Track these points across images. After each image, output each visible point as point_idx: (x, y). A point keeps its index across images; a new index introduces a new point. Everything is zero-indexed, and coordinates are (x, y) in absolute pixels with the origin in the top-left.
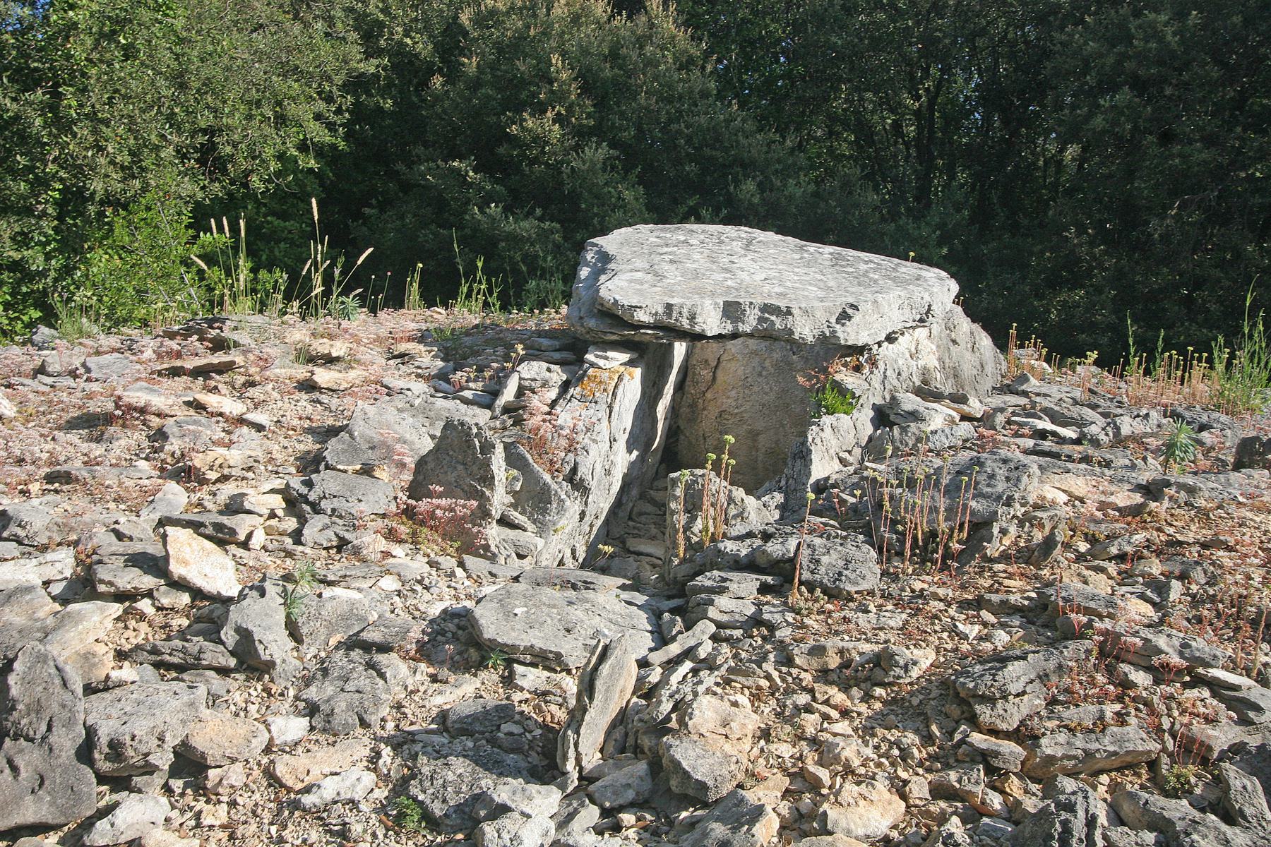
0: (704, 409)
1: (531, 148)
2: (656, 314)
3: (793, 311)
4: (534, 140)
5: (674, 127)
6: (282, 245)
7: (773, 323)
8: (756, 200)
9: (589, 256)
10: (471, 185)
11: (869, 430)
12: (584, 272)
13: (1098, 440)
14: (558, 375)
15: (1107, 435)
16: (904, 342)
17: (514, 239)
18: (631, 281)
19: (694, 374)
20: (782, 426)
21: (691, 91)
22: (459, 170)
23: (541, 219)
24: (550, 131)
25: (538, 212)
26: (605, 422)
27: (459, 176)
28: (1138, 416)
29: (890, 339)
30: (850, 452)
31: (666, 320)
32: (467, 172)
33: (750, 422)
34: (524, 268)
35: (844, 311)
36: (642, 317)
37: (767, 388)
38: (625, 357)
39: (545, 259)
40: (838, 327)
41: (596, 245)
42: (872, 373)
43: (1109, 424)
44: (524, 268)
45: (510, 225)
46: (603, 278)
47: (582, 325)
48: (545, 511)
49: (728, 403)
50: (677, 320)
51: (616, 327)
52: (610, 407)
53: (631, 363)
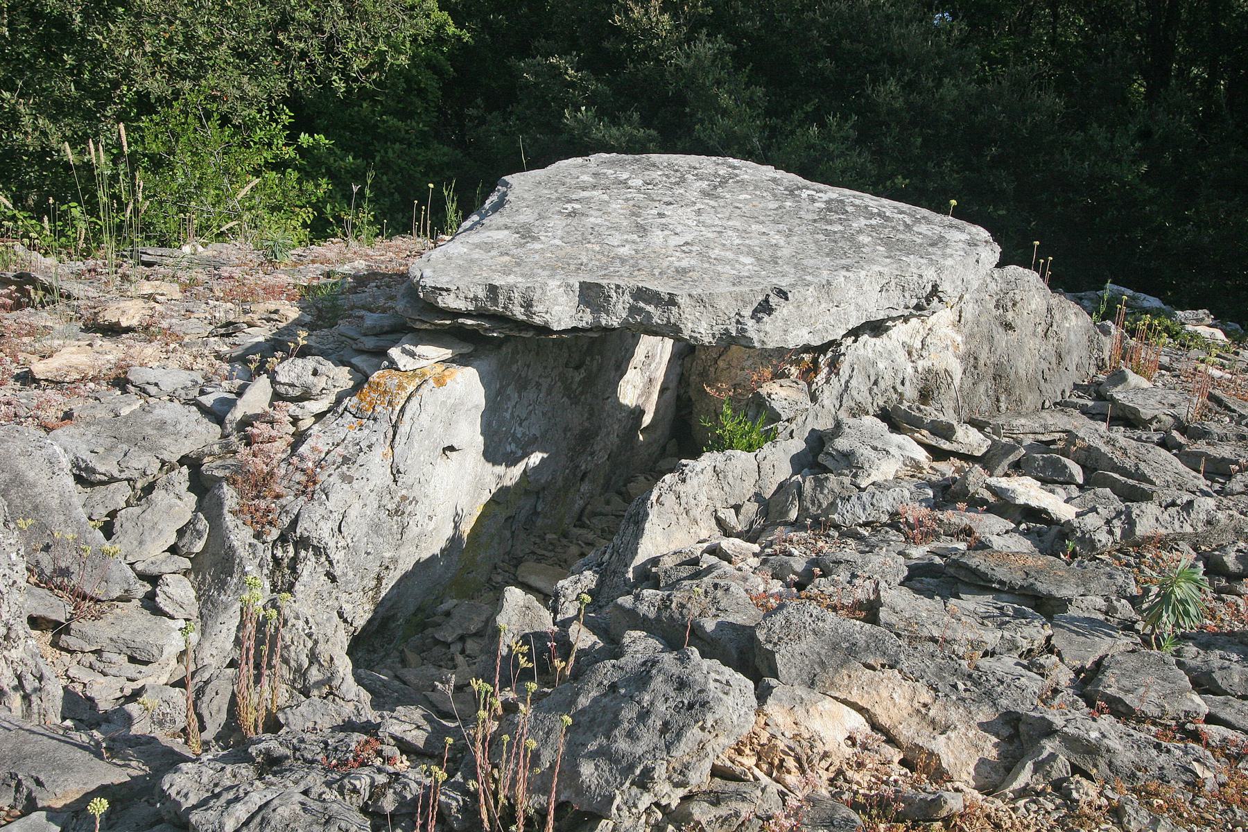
2: (476, 298)
3: (679, 300)
5: (808, 15)
6: (397, 146)
8: (897, 105)
10: (572, 85)
11: (784, 471)
13: (1092, 541)
14: (343, 377)
15: (1111, 532)
16: (899, 333)
26: (381, 450)
27: (556, 72)
28: (1173, 504)
29: (876, 328)
30: (737, 508)
38: (447, 353)
42: (828, 381)
43: (1119, 514)
48: (222, 586)
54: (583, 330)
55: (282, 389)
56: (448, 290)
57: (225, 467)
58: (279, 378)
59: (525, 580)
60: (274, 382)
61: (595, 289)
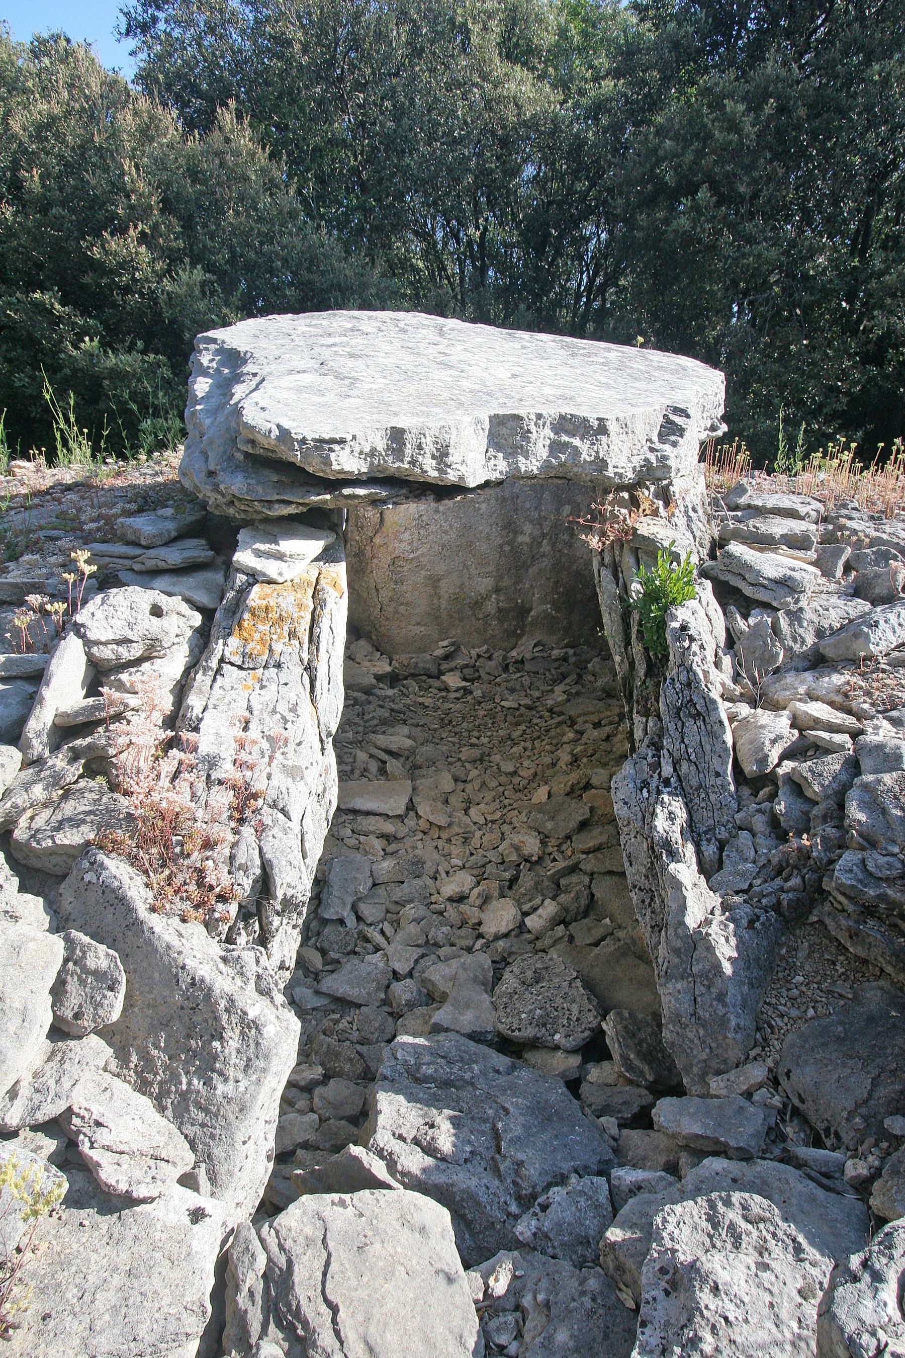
0: (373, 557)
1: (120, 275)
2: (373, 452)
4: (121, 265)
7: (576, 451)
9: (205, 359)
12: (201, 386)
17: (117, 375)
18: (299, 390)
19: (357, 516)
20: (466, 567)
21: (280, 212)
22: (43, 303)
23: (144, 352)
24: (137, 253)
25: (140, 344)
26: (306, 708)
27: (39, 307)
31: (393, 465)
32: (52, 305)
33: (428, 566)
34: (134, 407)
35: (668, 421)
36: (347, 462)
37: (446, 526)
38: (316, 546)
39: (155, 396)
40: (667, 447)
41: (214, 341)
44: (134, 407)
45: (112, 360)
46: (239, 391)
47: (216, 488)
48: (208, 1066)
49: (401, 547)
50: (413, 462)
51: (293, 487)
52: (310, 669)
53: (327, 556)
54: (500, 483)
55: (106, 653)
56: (342, 442)
57: (75, 822)
58: (92, 635)
59: (350, 806)
60: (88, 643)
61: (510, 424)
